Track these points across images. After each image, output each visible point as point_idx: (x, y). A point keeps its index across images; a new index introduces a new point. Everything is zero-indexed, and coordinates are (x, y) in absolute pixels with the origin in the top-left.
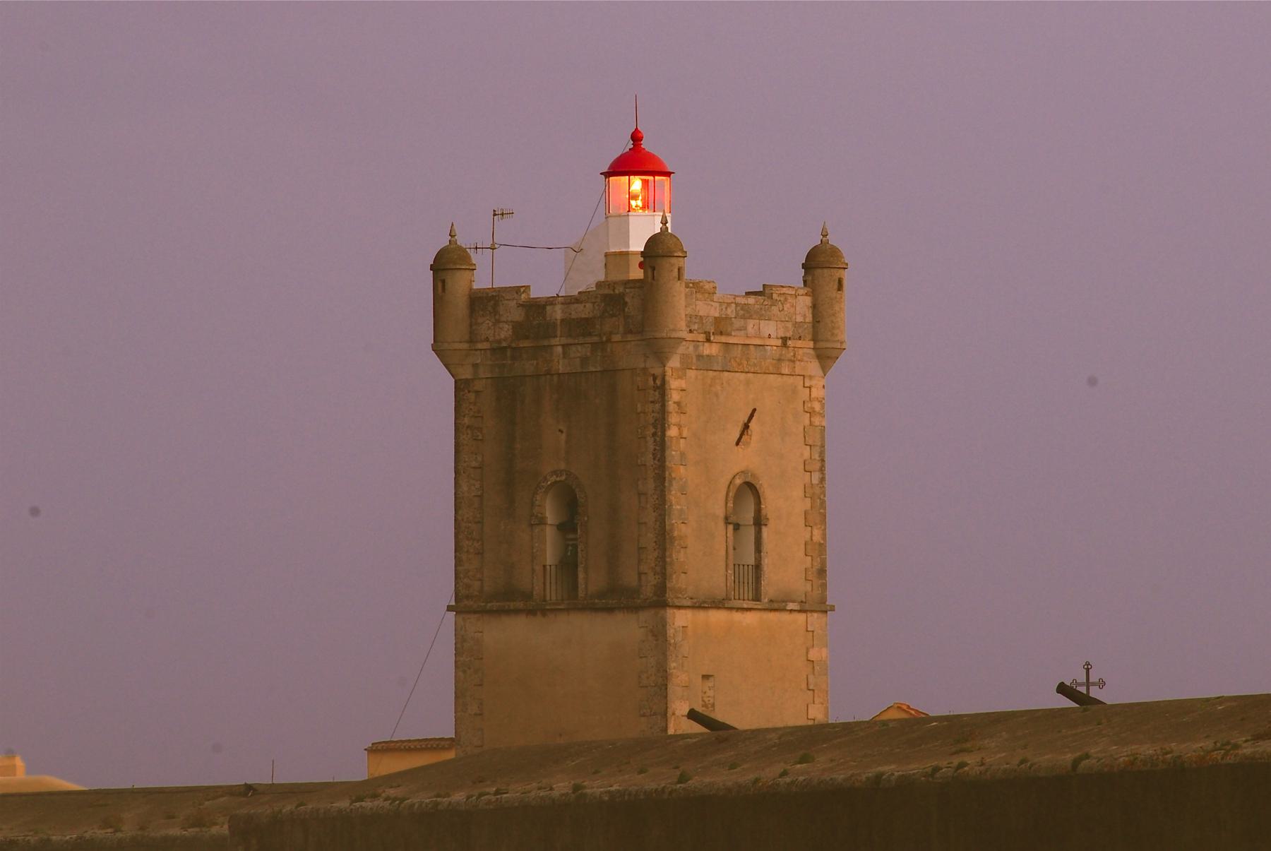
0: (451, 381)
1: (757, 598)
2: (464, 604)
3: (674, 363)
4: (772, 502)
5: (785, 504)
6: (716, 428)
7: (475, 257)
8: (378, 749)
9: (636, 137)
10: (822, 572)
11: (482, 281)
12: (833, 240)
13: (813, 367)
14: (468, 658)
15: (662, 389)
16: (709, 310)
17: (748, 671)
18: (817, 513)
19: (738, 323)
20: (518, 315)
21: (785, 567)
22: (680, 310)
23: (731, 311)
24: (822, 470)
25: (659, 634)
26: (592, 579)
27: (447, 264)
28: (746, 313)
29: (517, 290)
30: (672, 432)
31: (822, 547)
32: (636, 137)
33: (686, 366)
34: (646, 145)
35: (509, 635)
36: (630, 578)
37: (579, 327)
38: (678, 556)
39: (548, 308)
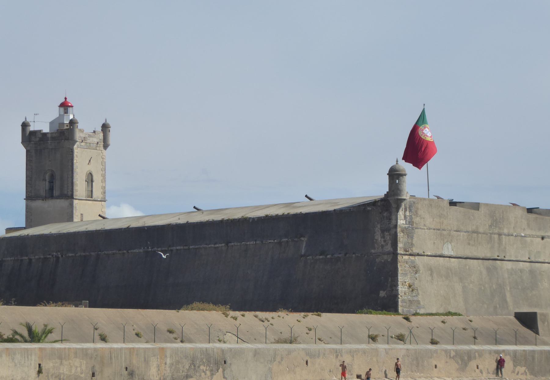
0: (25, 150)
1: (92, 197)
2: (29, 198)
3: (75, 146)
4: (95, 178)
5: (97, 178)
6: (83, 161)
7: (31, 124)
8: (9, 230)
9: (66, 99)
10: (105, 193)
11: (32, 128)
12: (108, 122)
13: (102, 148)
14: (29, 210)
15: (72, 151)
16: (82, 135)
17: (88, 215)
18: (104, 180)
19: (89, 138)
20: (40, 136)
21: (97, 193)
22: (78, 136)
23: (87, 136)
24: (105, 171)
25: (72, 205)
26: (56, 193)
27: (25, 125)
28: (90, 136)
29: (40, 131)
30: (75, 161)
31: (105, 187)
32: (66, 99)
33: (78, 147)
34: (67, 100)
35: (38, 204)
36: (66, 192)
37: (53, 138)
38: (75, 188)
39: (380, 211)
